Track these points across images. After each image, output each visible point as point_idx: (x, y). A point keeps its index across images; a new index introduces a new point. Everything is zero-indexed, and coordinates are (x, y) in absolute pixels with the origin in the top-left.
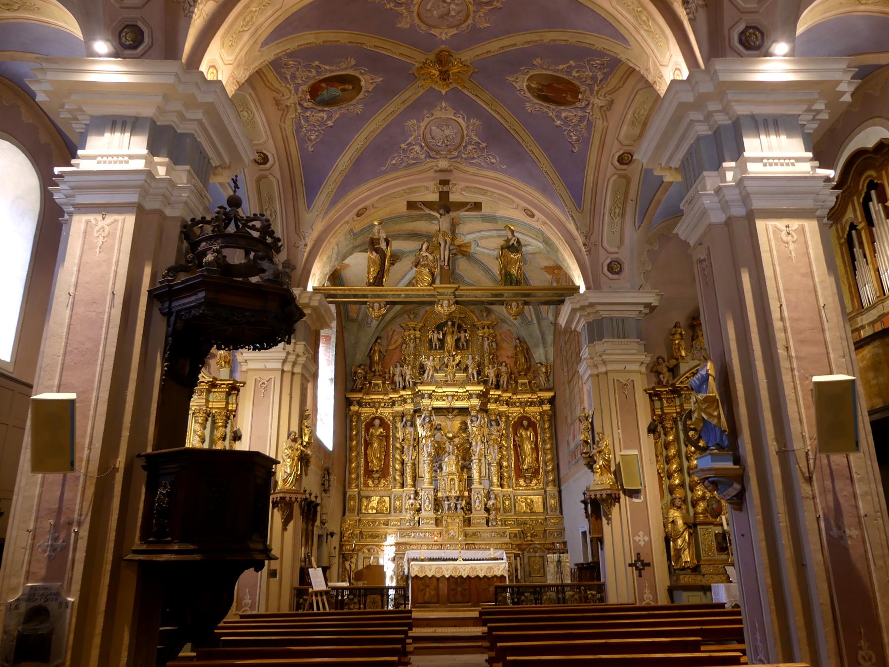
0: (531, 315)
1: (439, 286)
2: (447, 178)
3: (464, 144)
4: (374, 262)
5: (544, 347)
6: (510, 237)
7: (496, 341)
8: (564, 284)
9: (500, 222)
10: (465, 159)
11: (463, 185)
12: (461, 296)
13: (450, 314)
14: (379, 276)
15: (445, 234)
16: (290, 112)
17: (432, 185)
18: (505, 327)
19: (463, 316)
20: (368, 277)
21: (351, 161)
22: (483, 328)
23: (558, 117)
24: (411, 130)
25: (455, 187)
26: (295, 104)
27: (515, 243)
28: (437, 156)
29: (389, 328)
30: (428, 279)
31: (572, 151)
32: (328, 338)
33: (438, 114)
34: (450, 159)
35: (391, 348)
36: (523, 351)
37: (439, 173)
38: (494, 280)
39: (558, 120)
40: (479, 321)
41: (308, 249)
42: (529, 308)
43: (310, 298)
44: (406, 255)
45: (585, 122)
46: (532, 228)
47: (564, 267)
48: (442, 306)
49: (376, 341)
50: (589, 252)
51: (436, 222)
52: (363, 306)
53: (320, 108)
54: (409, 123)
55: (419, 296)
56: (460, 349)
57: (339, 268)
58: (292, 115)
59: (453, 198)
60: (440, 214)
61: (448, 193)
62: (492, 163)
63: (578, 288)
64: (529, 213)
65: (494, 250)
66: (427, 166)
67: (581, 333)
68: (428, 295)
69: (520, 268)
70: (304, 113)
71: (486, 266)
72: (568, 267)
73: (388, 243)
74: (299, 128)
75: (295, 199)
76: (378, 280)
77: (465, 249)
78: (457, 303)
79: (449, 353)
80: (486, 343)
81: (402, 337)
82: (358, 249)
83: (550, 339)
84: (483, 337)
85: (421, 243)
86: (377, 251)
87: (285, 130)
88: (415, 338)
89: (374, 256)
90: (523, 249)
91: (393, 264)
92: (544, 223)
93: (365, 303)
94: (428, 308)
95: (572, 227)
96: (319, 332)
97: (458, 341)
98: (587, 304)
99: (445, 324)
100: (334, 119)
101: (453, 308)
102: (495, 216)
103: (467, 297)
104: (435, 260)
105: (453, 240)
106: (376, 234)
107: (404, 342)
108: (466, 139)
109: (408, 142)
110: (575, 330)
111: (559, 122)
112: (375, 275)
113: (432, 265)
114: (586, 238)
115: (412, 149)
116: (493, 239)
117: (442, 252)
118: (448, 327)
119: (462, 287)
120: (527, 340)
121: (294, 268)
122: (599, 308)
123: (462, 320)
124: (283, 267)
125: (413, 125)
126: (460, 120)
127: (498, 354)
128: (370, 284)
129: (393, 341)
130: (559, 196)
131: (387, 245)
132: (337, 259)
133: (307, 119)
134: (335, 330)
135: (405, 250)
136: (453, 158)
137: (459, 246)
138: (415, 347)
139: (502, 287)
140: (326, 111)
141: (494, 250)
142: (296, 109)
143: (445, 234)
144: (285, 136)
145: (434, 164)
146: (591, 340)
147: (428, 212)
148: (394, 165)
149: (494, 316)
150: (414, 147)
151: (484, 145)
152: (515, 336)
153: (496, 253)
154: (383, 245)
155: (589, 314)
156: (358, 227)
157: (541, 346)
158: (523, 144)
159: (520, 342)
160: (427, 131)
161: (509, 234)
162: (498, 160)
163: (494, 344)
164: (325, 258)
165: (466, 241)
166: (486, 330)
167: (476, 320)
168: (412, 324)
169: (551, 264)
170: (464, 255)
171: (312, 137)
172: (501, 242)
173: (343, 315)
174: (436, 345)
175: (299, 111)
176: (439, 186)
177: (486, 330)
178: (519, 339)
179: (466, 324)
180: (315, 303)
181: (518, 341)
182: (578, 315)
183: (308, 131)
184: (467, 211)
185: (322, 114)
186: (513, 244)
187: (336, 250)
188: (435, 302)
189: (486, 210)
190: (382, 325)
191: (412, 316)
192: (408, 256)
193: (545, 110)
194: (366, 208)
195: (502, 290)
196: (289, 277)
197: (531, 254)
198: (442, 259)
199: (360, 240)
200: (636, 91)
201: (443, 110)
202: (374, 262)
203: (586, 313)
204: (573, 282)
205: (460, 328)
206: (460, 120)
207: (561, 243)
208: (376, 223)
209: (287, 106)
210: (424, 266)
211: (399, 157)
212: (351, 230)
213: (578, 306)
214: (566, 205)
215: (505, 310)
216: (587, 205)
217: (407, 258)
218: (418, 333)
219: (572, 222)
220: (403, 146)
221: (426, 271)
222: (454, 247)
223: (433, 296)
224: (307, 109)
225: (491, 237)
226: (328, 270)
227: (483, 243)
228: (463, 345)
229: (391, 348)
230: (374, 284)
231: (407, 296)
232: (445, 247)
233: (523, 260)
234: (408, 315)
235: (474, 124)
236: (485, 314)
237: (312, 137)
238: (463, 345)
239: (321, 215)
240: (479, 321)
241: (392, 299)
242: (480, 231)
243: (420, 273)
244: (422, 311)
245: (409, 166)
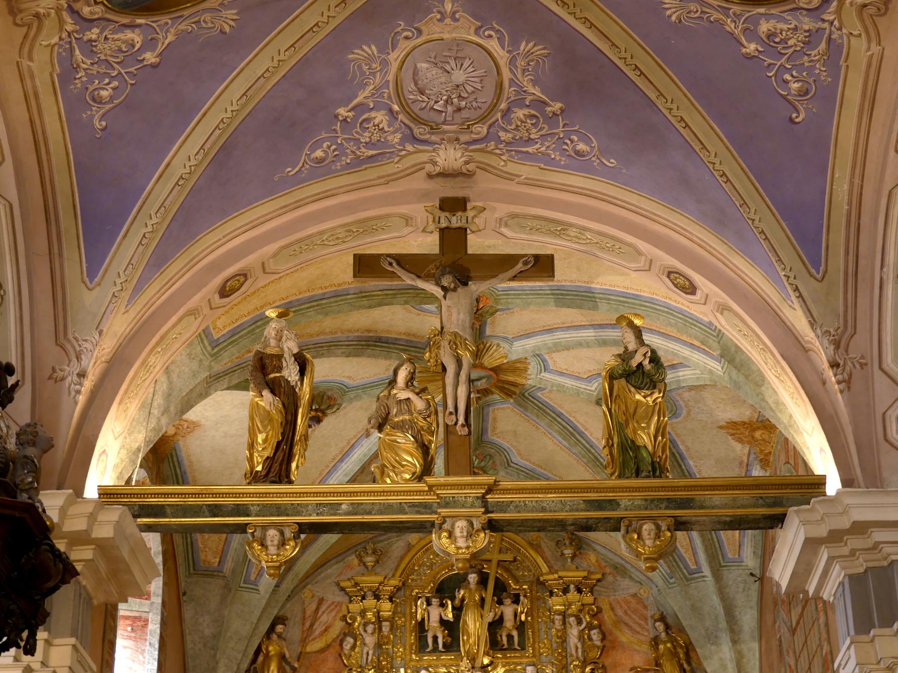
0: (695, 554)
1: (442, 480)
2: (460, 194)
3: (503, 106)
4: (267, 417)
5: (734, 642)
6: (632, 346)
7: (599, 627)
8: (784, 471)
9: (603, 306)
10: (508, 144)
11: (503, 209)
12: (502, 507)
13: (474, 556)
14: (280, 455)
15: (456, 342)
16: (44, 32)
17: (419, 211)
18: (626, 587)
19: (509, 557)
20: (251, 459)
21: (206, 155)
22: (566, 591)
23: (751, 33)
24: (363, 73)
25: (483, 215)
26: (58, 10)
27: (646, 362)
28: (434, 138)
29: (306, 593)
30: (412, 460)
31: (791, 120)
32: (138, 622)
33: (434, 29)
34: (468, 143)
35: (314, 646)
36: (674, 654)
37: (439, 180)
38: (593, 461)
39: (749, 42)
40: (552, 571)
41: (88, 384)
42: (691, 540)
43: (92, 518)
44: (352, 395)
45: (823, 46)
46: (690, 320)
47: (781, 421)
48: (451, 535)
49: (272, 629)
50: (847, 383)
51: (432, 307)
52: (237, 538)
53: (125, 20)
54: (357, 54)
55: (387, 509)
56: (502, 649)
57: (171, 431)
58: (50, 37)
59: (476, 244)
60: (444, 289)
61: (463, 231)
62: (578, 153)
63: (820, 482)
64: (681, 281)
65: (589, 379)
66: (409, 162)
67: (832, 606)
68: (413, 505)
69: (661, 430)
70: (82, 31)
71: (569, 422)
72: (792, 423)
73: (303, 366)
74: (69, 71)
75: (54, 255)
76: (276, 466)
77: (511, 378)
78: (492, 526)
79: (473, 660)
80: (574, 632)
81: (344, 618)
82: (225, 382)
83: (748, 619)
84: (564, 615)
85: (395, 363)
86: (275, 387)
87: (32, 77)
88: (379, 620)
89: (267, 400)
90: (670, 376)
91: (318, 420)
92: (723, 308)
93: (242, 528)
94: (413, 538)
95: (798, 319)
96: (115, 608)
97: (495, 625)
98: (847, 525)
99: (459, 580)
100: (160, 48)
101: (482, 540)
102: (590, 291)
103: (518, 509)
104: (431, 411)
105: (477, 355)
106: (273, 342)
107: (349, 631)
108: (509, 91)
109: (355, 102)
110: (817, 598)
111: (753, 46)
112: (268, 453)
113: (422, 423)
114: (837, 345)
115: (367, 120)
116: (585, 352)
117: (449, 390)
118: (467, 587)
119: (504, 484)
120: (685, 623)
121: (49, 445)
122: (879, 536)
123: (507, 570)
124: (20, 443)
125: (370, 59)
126: (493, 45)
127: (608, 662)
128: (255, 478)
129: (318, 629)
130: (761, 238)
131: (302, 372)
132: (166, 411)
133: (89, 47)
134: (159, 600)
135: (350, 383)
136: (475, 141)
137: (496, 370)
138: (379, 645)
139: (614, 482)
140: (139, 26)
141: (589, 379)
142: (61, 22)
143: (456, 342)
144: (31, 92)
145: (424, 157)
146: (863, 624)
147: (409, 282)
148: (321, 161)
149: (593, 558)
150: (373, 114)
151: (557, 106)
152: (651, 612)
153: (597, 386)
154: (290, 372)
155: (853, 553)
156: (222, 325)
157: (725, 639)
158: (660, 103)
159: (667, 627)
160: (407, 76)
161: (631, 343)
162: (595, 144)
163: (595, 635)
164: (133, 407)
165: (514, 357)
166: (573, 595)
167: (545, 569)
168: (370, 581)
169: (742, 414)
170: (509, 394)
171: (104, 93)
172: (608, 358)
173: (180, 559)
174: (435, 638)
175: (69, 28)
176: (438, 213)
177: (573, 595)
178: (662, 619)
179: (517, 581)
180: (104, 531)
181: (660, 626)
182: (824, 555)
183: (91, 78)
184: (514, 278)
185: (129, 35)
186: (640, 365)
187: (163, 386)
188: (433, 524)
189: (564, 274)
190: (289, 584)
191: (370, 560)
192: (358, 397)
193: (716, 15)
194: (244, 275)
195: (613, 489)
196: (36, 471)
197: (692, 388)
198: (451, 408)
199: (228, 358)
200: (885, 193)
201: (448, 21)
202: (267, 417)
203: (845, 551)
204: (805, 464)
205: (501, 589)
206: (493, 45)
207: (771, 362)
208: (271, 313)
209: (37, 16)
210: (400, 427)
211: (333, 140)
212: (207, 332)
213: (822, 531)
214: (780, 260)
215: (623, 545)
216: (837, 261)
217: (357, 404)
218: (386, 607)
219: (797, 305)
220: (342, 111)
221: (405, 440)
222: (483, 373)
223: (426, 507)
224: (90, 22)
225: (580, 344)
226: (140, 439)
227: (559, 360)
228: (510, 637)
229: (314, 646)
230: (264, 477)
231: (356, 508)
232: (457, 375)
233: (670, 407)
234: (360, 558)
235: (529, 53)
236: (568, 552)
237: (104, 93)
238: (510, 637)
239: (126, 295)
240: (552, 571)
241: (314, 518)
242: (550, 330)
243: (392, 446)
244: (398, 544)
245: (359, 163)
